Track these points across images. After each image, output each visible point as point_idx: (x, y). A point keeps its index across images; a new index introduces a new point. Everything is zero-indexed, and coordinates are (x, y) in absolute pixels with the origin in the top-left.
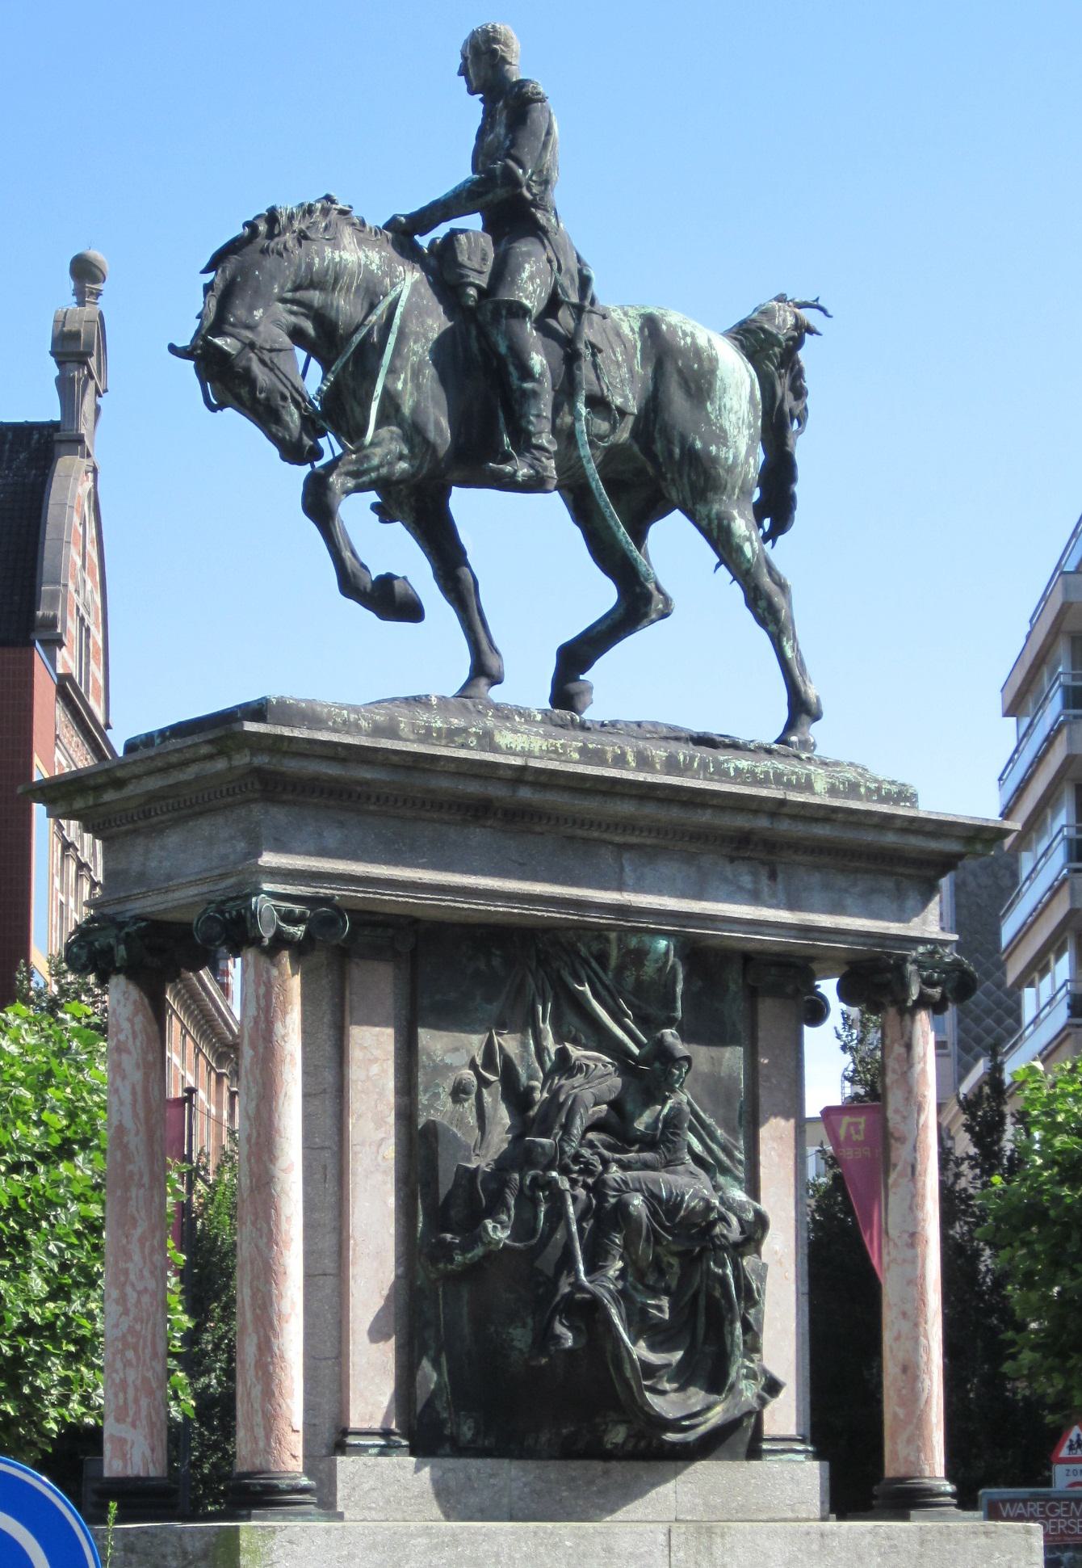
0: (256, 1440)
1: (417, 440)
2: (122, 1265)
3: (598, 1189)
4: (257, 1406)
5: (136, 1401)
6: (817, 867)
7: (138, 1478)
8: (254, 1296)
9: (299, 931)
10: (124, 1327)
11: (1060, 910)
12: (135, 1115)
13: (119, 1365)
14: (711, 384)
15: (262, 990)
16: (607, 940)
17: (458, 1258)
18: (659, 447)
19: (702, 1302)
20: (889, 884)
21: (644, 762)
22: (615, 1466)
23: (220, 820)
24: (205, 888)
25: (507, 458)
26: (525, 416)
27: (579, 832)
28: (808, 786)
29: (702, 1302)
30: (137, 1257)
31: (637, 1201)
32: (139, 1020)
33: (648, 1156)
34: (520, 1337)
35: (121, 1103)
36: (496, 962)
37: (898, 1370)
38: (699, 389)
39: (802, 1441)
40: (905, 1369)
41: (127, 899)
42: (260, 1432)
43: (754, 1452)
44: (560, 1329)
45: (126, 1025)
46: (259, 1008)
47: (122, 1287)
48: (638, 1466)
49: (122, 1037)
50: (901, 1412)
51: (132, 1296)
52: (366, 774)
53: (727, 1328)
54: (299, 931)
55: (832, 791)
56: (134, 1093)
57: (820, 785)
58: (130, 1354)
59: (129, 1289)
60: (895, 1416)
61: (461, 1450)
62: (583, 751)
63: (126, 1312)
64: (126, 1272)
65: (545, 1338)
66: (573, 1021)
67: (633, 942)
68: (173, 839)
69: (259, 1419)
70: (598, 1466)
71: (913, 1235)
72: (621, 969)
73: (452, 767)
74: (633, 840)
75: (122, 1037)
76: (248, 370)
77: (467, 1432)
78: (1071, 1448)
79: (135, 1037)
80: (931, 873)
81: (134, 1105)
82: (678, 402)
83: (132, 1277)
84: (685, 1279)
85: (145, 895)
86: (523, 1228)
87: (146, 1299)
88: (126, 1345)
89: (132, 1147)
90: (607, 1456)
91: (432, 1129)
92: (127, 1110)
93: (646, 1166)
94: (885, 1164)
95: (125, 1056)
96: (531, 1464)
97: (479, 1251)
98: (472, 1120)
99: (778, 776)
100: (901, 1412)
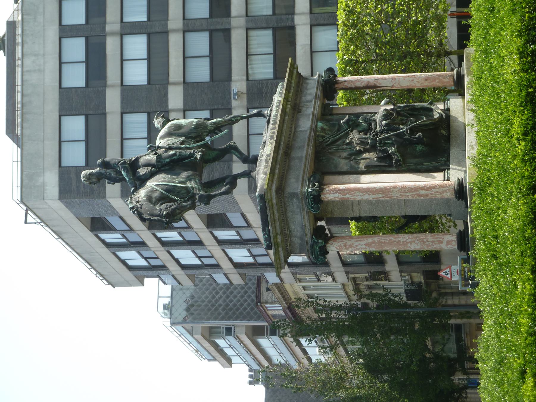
0: (446, 190)
1: (191, 177)
2: (401, 243)
3: (381, 132)
4: (438, 190)
5: (437, 238)
6: (301, 98)
7: (457, 238)
8: (410, 192)
9: (316, 184)
10: (418, 242)
11: (290, 340)
12: (363, 241)
13: (427, 243)
14: (178, 124)
15: (332, 192)
16: (319, 135)
17: (399, 158)
18: (193, 135)
19: (410, 112)
20: (305, 85)
21: (274, 128)
22: (451, 133)
23: (288, 208)
24: (305, 212)
25: (196, 158)
26: (185, 155)
27: (292, 137)
28: (280, 101)
29: (410, 112)
30: (399, 239)
31: (384, 122)
32: (338, 240)
33: (373, 124)
34: (419, 148)
35: (360, 244)
36: (324, 158)
37: (426, 82)
38: (179, 127)
39: (445, 103)
40: (426, 80)
41: (307, 242)
42: (444, 189)
43: (448, 110)
44: (417, 136)
45: (339, 244)
46: (336, 193)
47: (408, 243)
48: (451, 129)
49: (342, 245)
50: (437, 81)
51: (410, 240)
52: (277, 171)
53: (416, 107)
54: (316, 184)
55: (281, 97)
56: (357, 241)
57: (280, 99)
58: (425, 240)
59: (408, 241)
60: (438, 82)
61: (448, 160)
62: (271, 139)
63: (414, 242)
64: (404, 242)
65: (419, 141)
66: (339, 143)
67: (319, 129)
68: (292, 227)
69: (441, 189)
70: (452, 136)
71: (392, 79)
72: (325, 133)
73: (274, 163)
74: (293, 128)
75: (342, 245)
76: (172, 209)
77: (443, 159)
78: (447, 275)
79: (342, 241)
80: (302, 79)
81: (360, 241)
82: (182, 131)
83: (405, 240)
84: (405, 116)
85: (306, 235)
86: (392, 145)
87: (410, 237)
88: (423, 241)
89: (371, 241)
90: (449, 135)
91: (366, 167)
92: (361, 243)
93: (376, 124)
94: (375, 87)
95: (347, 244)
96: (451, 148)
97: (397, 154)
98: (364, 161)
99: (277, 106)
100: (437, 81)
